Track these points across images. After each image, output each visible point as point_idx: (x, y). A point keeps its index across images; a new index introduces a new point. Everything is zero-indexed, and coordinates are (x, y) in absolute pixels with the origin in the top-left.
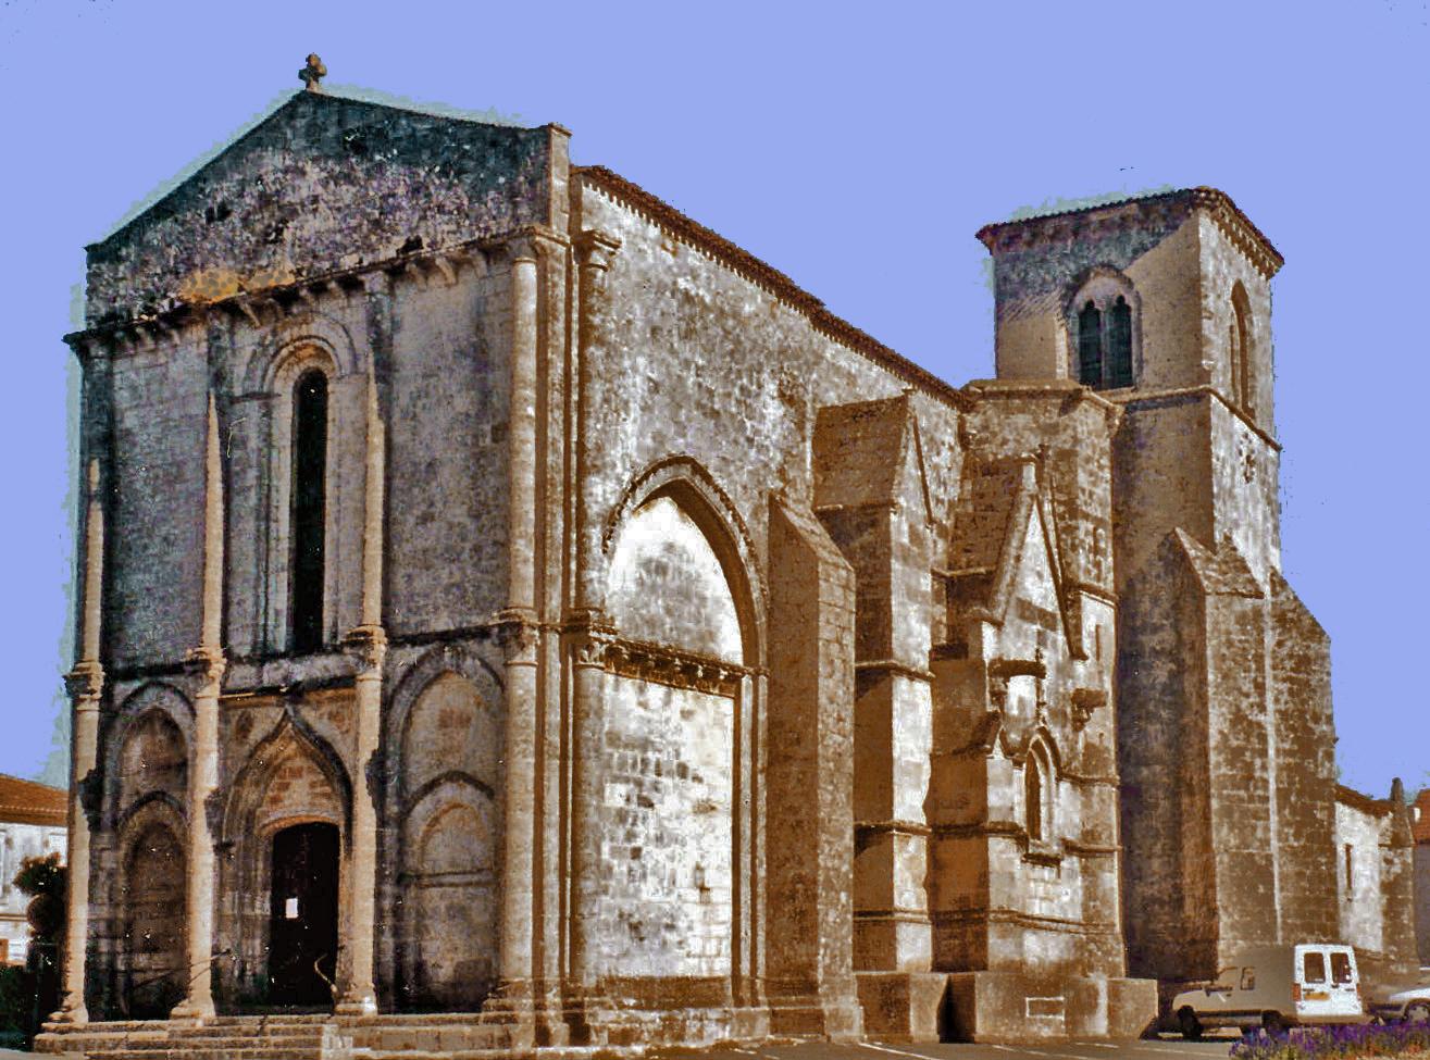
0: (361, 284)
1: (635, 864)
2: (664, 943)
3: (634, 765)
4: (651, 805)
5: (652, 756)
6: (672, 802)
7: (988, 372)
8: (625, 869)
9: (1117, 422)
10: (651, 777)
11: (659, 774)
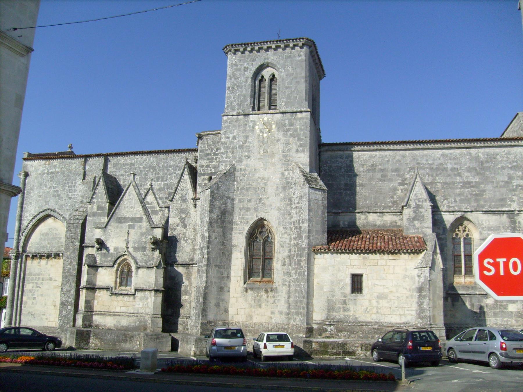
0: (278, 338)
1: (34, 301)
2: (42, 319)
3: (36, 279)
4: (40, 288)
5: (41, 277)
6: (45, 287)
7: (324, 140)
8: (31, 302)
9: (335, 357)
10: (40, 281)
11: (43, 280)
